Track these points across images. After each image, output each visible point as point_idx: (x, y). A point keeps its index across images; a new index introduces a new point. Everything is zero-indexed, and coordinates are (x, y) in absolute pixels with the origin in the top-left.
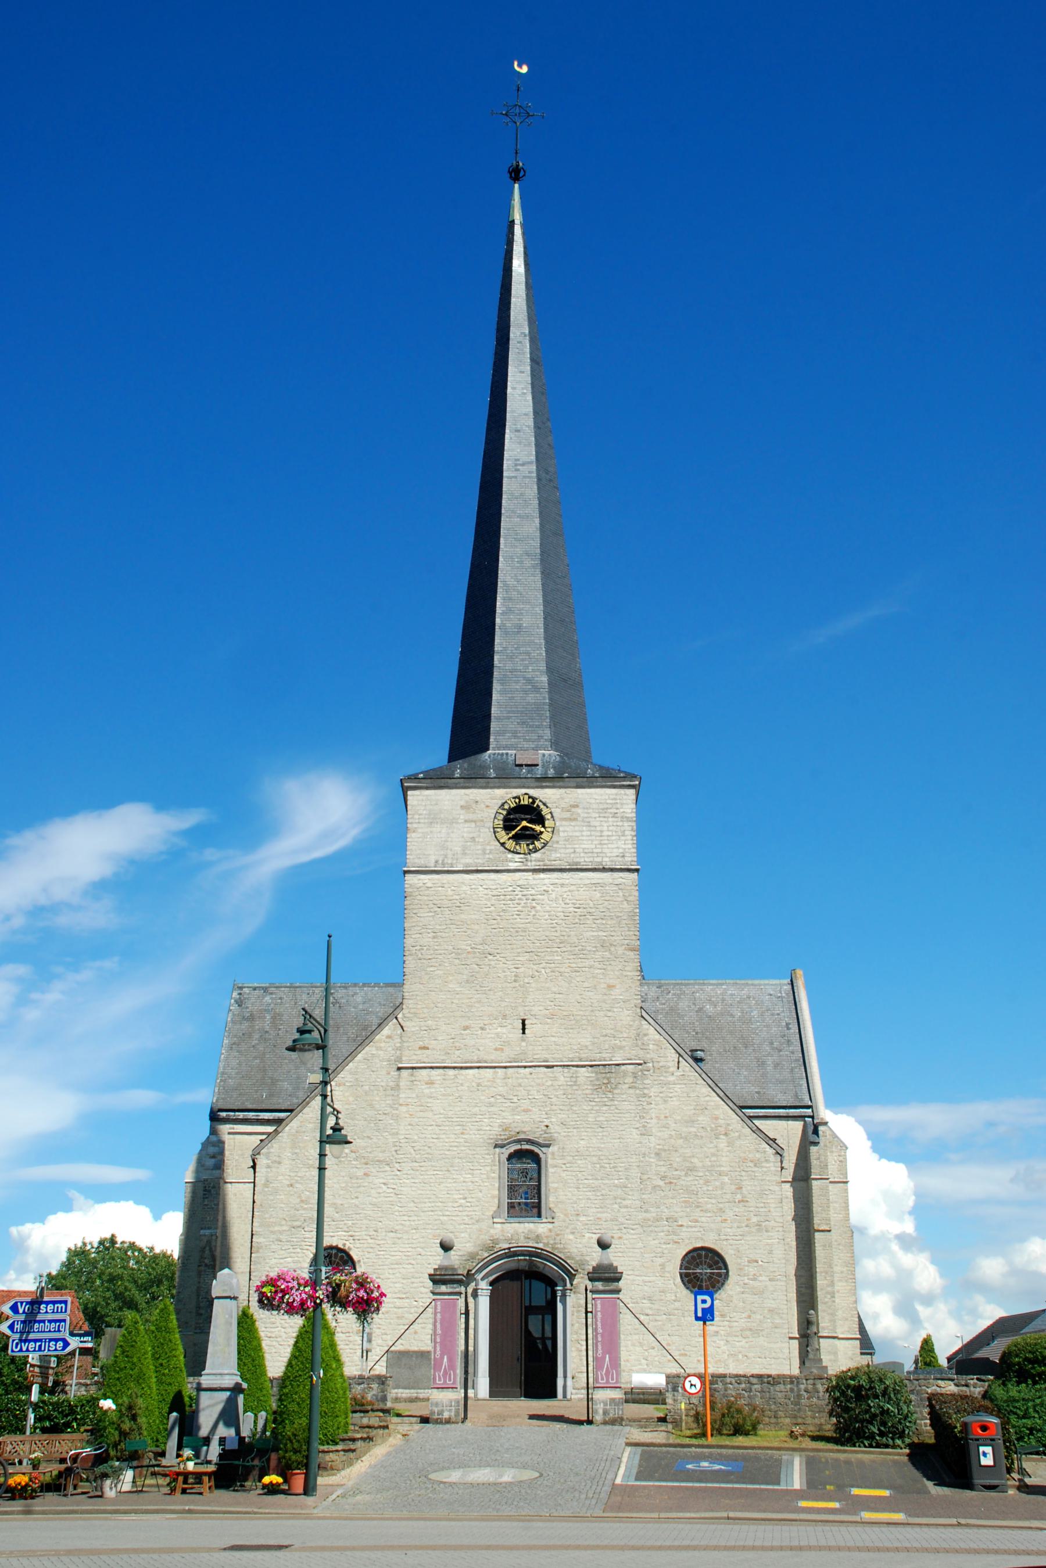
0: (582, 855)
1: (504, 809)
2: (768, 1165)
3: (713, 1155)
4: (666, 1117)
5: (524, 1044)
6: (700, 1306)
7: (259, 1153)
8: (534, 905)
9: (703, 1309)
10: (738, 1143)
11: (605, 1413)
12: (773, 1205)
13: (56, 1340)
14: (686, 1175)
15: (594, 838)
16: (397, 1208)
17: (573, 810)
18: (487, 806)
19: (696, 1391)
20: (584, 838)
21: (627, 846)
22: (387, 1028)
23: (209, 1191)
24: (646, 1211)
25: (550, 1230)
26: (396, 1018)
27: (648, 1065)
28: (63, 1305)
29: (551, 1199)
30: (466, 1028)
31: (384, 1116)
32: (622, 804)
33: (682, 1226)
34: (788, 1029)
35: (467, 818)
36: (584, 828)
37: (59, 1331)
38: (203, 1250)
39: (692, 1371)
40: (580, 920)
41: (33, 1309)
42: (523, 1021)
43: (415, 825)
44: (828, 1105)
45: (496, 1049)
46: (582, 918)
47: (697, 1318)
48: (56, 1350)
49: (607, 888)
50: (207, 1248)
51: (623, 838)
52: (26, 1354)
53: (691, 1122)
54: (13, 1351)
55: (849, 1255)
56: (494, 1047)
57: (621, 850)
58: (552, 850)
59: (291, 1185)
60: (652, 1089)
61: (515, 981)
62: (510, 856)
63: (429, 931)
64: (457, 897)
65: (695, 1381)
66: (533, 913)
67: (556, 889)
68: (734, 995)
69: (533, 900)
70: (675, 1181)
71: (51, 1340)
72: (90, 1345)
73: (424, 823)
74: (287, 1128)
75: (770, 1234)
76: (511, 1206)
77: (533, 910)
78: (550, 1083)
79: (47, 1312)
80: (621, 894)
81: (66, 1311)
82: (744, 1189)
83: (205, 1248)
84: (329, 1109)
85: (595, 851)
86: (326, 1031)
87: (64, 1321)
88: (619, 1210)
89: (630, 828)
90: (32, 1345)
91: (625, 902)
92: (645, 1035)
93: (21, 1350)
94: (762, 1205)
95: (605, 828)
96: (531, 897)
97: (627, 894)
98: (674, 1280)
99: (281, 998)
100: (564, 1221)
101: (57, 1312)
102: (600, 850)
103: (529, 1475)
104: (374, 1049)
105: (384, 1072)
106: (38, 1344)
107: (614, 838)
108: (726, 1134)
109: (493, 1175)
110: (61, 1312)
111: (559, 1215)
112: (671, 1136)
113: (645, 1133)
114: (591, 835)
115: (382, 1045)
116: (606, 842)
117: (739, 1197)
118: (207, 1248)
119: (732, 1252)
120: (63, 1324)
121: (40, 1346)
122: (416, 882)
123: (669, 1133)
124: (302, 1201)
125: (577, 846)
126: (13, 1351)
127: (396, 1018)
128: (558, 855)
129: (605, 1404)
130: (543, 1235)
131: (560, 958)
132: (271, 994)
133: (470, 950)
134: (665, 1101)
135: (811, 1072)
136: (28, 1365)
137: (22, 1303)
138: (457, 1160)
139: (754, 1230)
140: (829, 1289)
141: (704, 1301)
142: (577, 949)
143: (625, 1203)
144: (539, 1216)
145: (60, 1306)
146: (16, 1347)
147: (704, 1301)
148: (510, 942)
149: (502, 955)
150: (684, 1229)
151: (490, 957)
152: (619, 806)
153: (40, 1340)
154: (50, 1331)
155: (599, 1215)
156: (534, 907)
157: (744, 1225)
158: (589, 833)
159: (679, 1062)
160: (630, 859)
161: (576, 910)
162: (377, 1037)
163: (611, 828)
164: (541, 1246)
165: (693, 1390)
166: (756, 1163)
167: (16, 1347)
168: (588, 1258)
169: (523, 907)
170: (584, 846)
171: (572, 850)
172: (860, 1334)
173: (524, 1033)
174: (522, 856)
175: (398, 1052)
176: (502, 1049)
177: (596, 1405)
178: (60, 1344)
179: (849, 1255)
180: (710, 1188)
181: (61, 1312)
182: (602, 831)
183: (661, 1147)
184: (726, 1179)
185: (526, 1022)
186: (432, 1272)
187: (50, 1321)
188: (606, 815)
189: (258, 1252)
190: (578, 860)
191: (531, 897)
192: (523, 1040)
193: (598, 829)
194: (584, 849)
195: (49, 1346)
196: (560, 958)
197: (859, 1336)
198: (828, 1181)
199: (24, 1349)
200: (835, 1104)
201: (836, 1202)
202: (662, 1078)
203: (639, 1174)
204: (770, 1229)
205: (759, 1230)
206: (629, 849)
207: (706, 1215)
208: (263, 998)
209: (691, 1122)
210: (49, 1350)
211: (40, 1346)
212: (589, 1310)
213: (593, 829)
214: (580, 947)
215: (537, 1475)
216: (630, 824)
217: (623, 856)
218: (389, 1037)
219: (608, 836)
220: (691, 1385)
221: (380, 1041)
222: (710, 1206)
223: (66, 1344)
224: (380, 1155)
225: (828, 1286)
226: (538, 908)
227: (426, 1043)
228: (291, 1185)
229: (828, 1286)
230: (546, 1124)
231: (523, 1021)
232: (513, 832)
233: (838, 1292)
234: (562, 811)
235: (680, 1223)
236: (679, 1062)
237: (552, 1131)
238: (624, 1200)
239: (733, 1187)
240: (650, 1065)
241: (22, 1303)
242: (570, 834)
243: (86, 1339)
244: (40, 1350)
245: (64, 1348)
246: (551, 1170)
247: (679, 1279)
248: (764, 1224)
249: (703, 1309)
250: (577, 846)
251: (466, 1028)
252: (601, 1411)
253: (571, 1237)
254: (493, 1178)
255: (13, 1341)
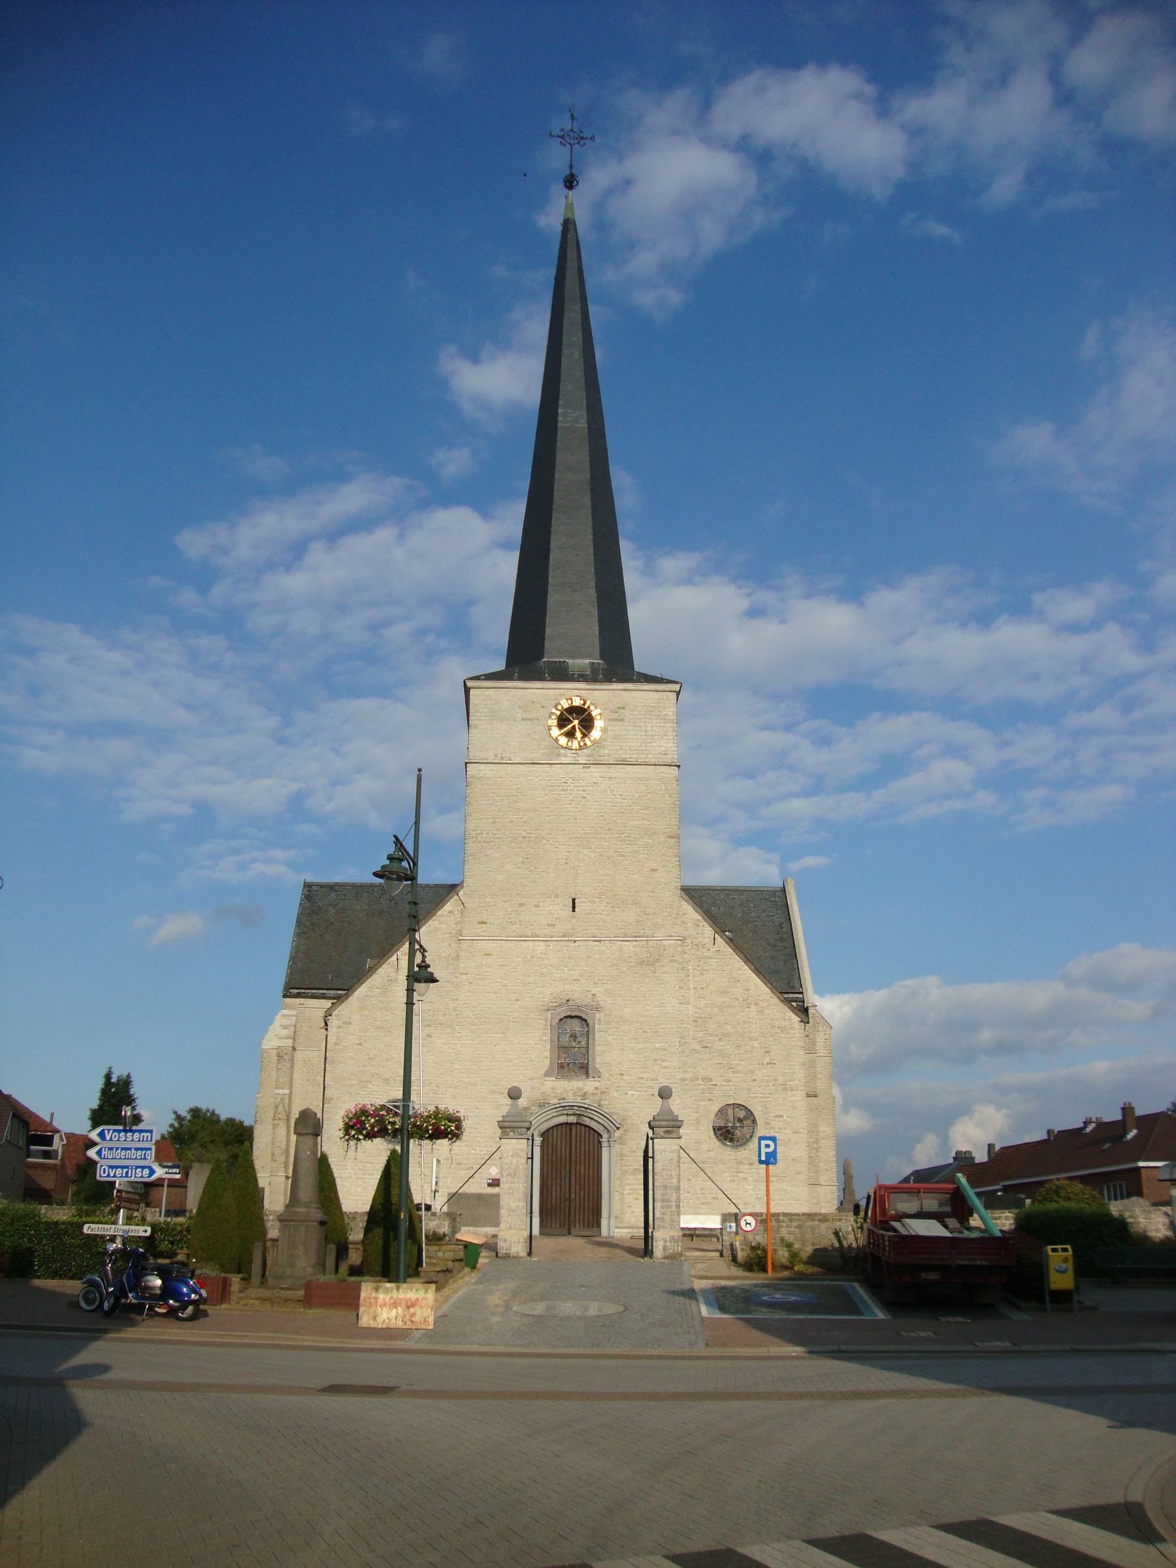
0: (628, 752)
1: (557, 709)
2: (793, 1032)
3: (745, 1022)
4: (702, 988)
5: (574, 921)
6: (764, 1150)
7: (331, 1015)
8: (585, 795)
9: (766, 1153)
10: (767, 1012)
11: (665, 1249)
12: (798, 1068)
13: (143, 1168)
14: (720, 1040)
15: (639, 737)
16: (457, 1066)
17: (620, 711)
18: (543, 707)
19: (751, 1229)
20: (630, 737)
21: (669, 745)
22: (449, 904)
23: (282, 1057)
24: (684, 1072)
25: (596, 1088)
26: (458, 895)
27: (687, 941)
28: (149, 1134)
29: (598, 1060)
30: (521, 905)
31: (446, 984)
32: (665, 708)
33: (716, 1085)
34: (782, 928)
35: (524, 717)
36: (630, 728)
37: (145, 1158)
38: (277, 1107)
39: (748, 1211)
40: (626, 809)
41: (119, 1137)
42: (574, 900)
43: (477, 722)
44: (815, 992)
45: (549, 925)
46: (628, 808)
47: (761, 1162)
48: (142, 1177)
49: (651, 782)
50: (281, 1105)
51: (665, 737)
52: (113, 1179)
53: (725, 992)
54: (100, 1176)
55: (831, 1117)
56: (547, 923)
57: (663, 749)
58: (601, 747)
59: (360, 1044)
60: (691, 963)
61: (566, 863)
62: (562, 751)
63: (489, 817)
64: (514, 787)
65: (750, 1219)
66: (584, 803)
67: (605, 782)
68: (735, 899)
69: (584, 791)
70: (710, 1045)
71: (137, 1167)
72: (178, 1176)
73: (484, 720)
74: (356, 993)
75: (794, 1092)
76: (561, 1066)
77: (583, 800)
78: (597, 956)
79: (133, 1140)
80: (663, 787)
81: (151, 1140)
82: (771, 1053)
83: (279, 1105)
84: (417, 947)
85: (640, 748)
86: (415, 864)
87: (150, 1149)
88: (659, 1071)
89: (672, 729)
90: (119, 1171)
91: (667, 795)
92: (684, 914)
93: (108, 1176)
94: (788, 1067)
95: (650, 728)
96: (582, 788)
97: (668, 788)
98: (708, 1133)
99: (345, 895)
100: (609, 1080)
101: (143, 1141)
102: (644, 748)
103: (611, 1309)
104: (437, 922)
105: (446, 944)
106: (125, 1170)
107: (657, 737)
108: (756, 1004)
109: (544, 1038)
110: (147, 1141)
111: (605, 1074)
112: (707, 1006)
113: (684, 1001)
114: (637, 735)
115: (445, 919)
116: (650, 741)
117: (767, 1060)
118: (281, 1105)
119: (760, 1108)
120: (149, 1152)
121: (127, 1172)
122: (477, 772)
123: (706, 1002)
124: (370, 1059)
125: (624, 744)
126: (100, 1176)
127: (458, 895)
128: (607, 752)
129: (666, 1241)
130: (590, 1092)
131: (607, 844)
132: (337, 891)
133: (526, 835)
134: (702, 974)
135: (801, 964)
136: (115, 1191)
137: (109, 1130)
138: (512, 1024)
139: (780, 1088)
140: (814, 1145)
141: (767, 1146)
142: (623, 836)
143: (665, 1064)
144: (587, 1074)
145: (146, 1135)
146: (104, 1173)
147: (767, 1146)
148: (561, 829)
149: (554, 840)
150: (717, 1088)
151: (544, 842)
152: (661, 709)
153: (127, 1167)
154: (136, 1158)
155: (640, 1076)
156: (585, 797)
157: (771, 1084)
158: (634, 733)
159: (714, 939)
160: (671, 756)
161: (622, 801)
162: (440, 912)
163: (654, 729)
164: (587, 1101)
165: (748, 1228)
166: (783, 1029)
167: (104, 1173)
168: (630, 1113)
169: (574, 797)
170: (630, 744)
171: (620, 747)
172: (838, 1182)
173: (574, 911)
174: (574, 751)
175: (459, 926)
176: (554, 925)
177: (657, 1241)
178: (146, 1171)
179: (831, 1117)
180: (742, 1052)
181: (147, 1141)
182: (646, 731)
183: (697, 1015)
184: (756, 1044)
185: (576, 901)
186: (501, 1119)
187: (137, 1149)
188: (650, 717)
189: (329, 1103)
190: (625, 756)
191: (582, 788)
192: (573, 917)
193: (643, 729)
194: (630, 746)
195: (136, 1173)
196: (607, 844)
197: (837, 1184)
198: (816, 1055)
199: (112, 1175)
200: (821, 993)
201: (822, 1073)
202: (699, 953)
203: (678, 1039)
204: (794, 1088)
205: (785, 1089)
206: (671, 747)
207: (738, 1075)
208: (329, 895)
209: (725, 992)
210: (135, 1177)
211: (127, 1172)
212: (531, 1160)
213: (638, 729)
214: (626, 834)
215: (622, 1308)
216: (671, 725)
217: (665, 754)
218: (450, 912)
219: (652, 736)
220: (747, 1223)
221: (442, 916)
222: (741, 1068)
223: (152, 1172)
224: (442, 1018)
225: (814, 1143)
226: (589, 797)
227: (484, 918)
228: (360, 1044)
229: (814, 1143)
230: (592, 993)
231: (574, 900)
232: (565, 729)
233: (821, 1148)
234: (611, 712)
235: (714, 1083)
236: (714, 939)
237: (599, 1000)
238: (664, 1061)
239: (762, 1051)
240: (689, 941)
241: (109, 1130)
242: (618, 733)
243: (174, 1170)
244: (127, 1176)
245: (150, 1175)
246: (597, 1034)
247: (712, 1132)
248: (789, 1083)
249: (766, 1153)
250: (624, 744)
251: (521, 905)
252: (661, 1248)
253: (615, 1094)
254: (545, 1041)
255: (101, 1166)
